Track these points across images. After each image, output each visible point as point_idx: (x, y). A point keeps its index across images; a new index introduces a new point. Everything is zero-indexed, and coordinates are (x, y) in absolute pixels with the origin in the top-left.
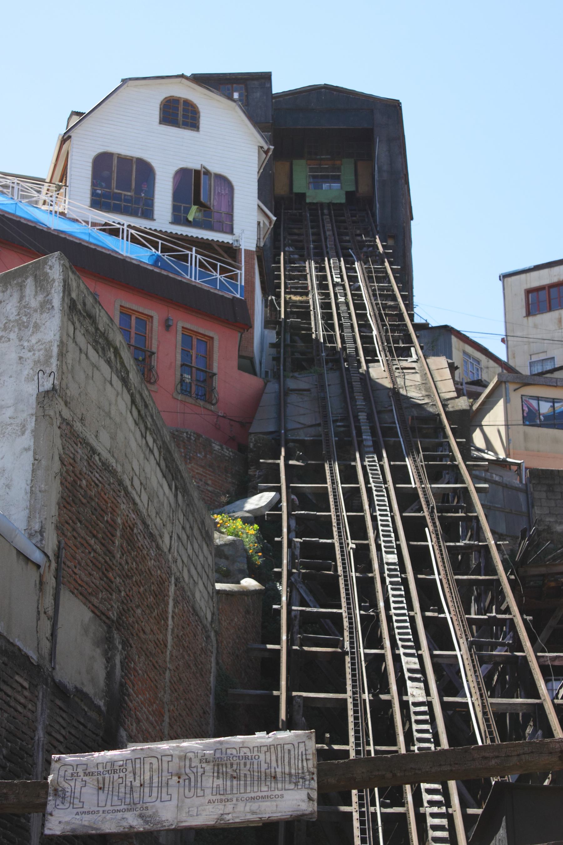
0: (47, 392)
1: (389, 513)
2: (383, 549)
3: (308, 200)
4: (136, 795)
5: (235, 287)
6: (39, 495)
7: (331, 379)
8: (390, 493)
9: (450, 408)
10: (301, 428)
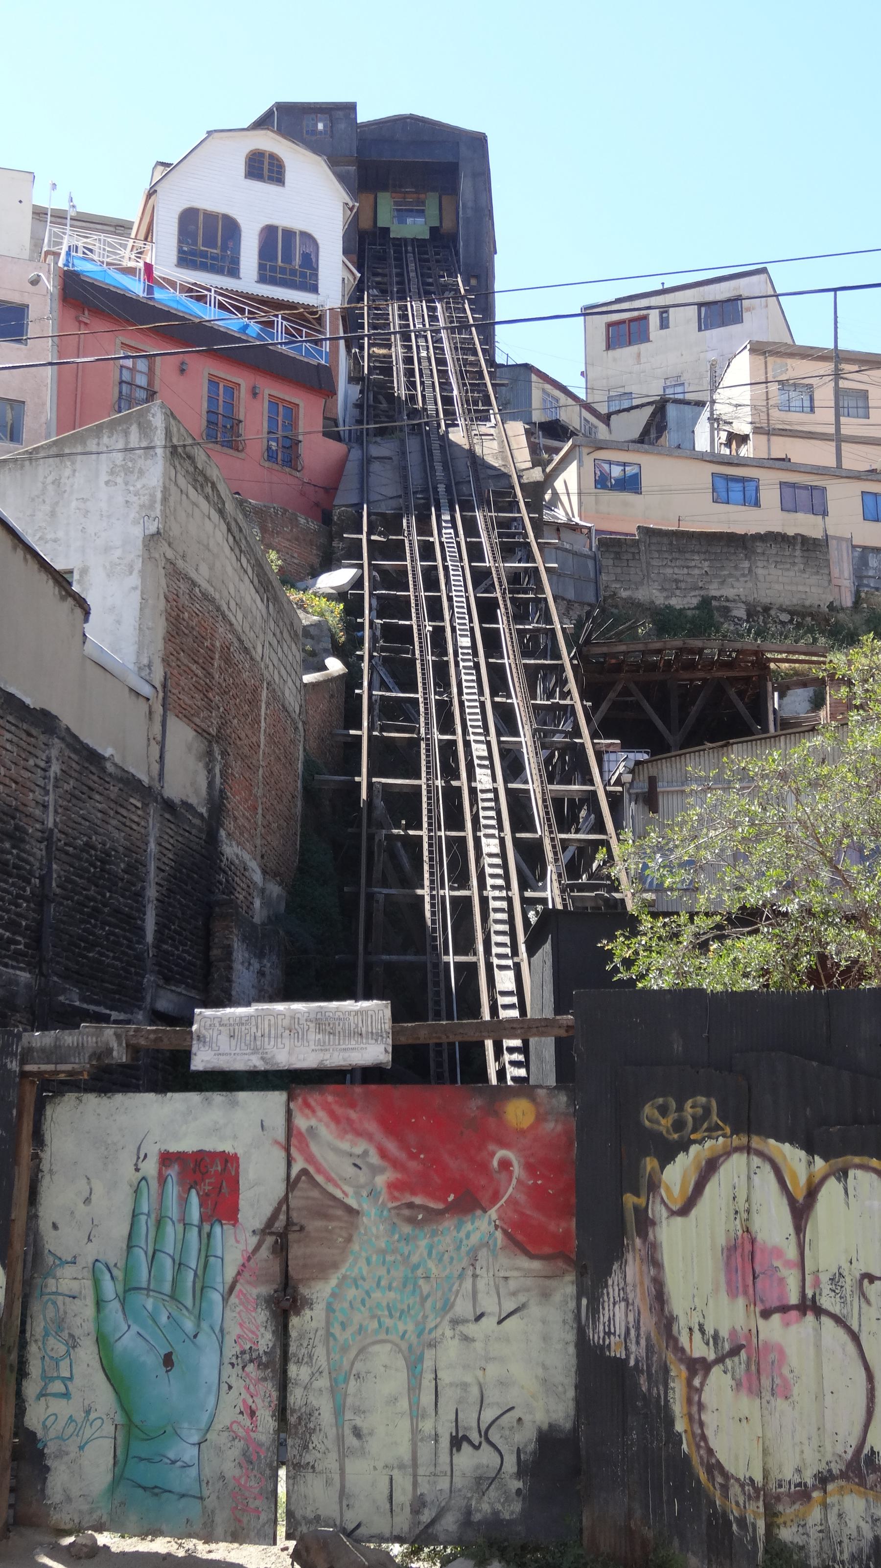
0: (153, 535)
4: (258, 1043)
5: (320, 353)
6: (147, 632)
9: (525, 480)
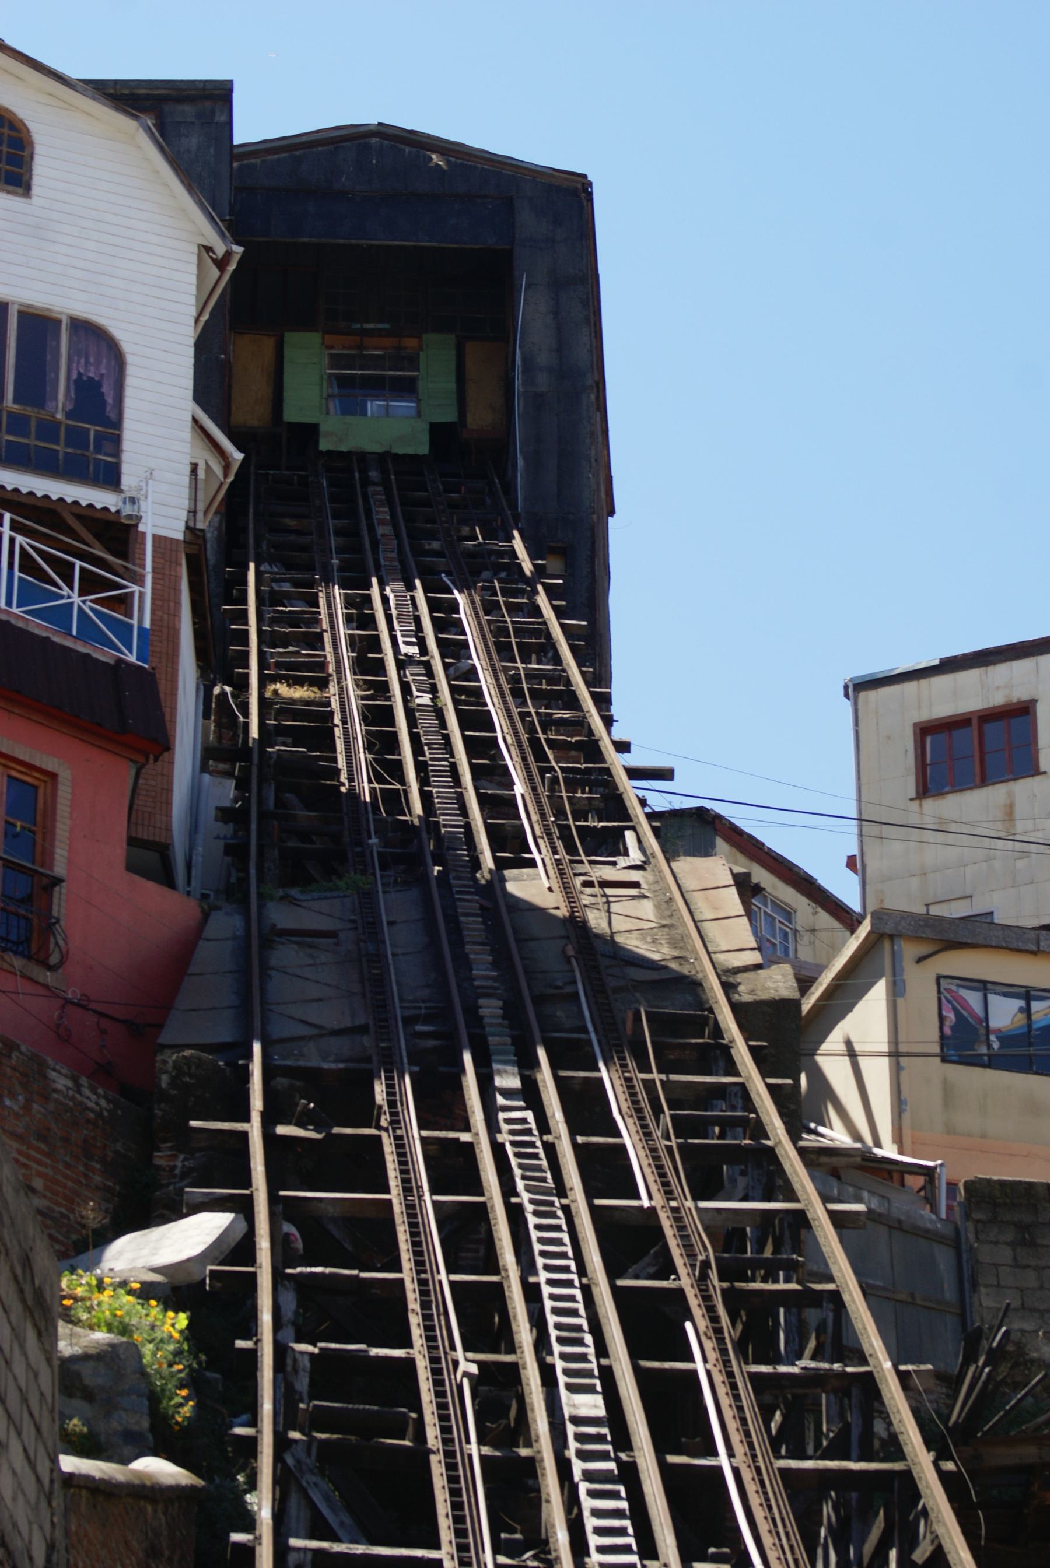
2: (562, 1380)
3: (324, 445)
5: (124, 631)
7: (396, 907)
8: (577, 1221)
9: (744, 995)
10: (311, 1038)
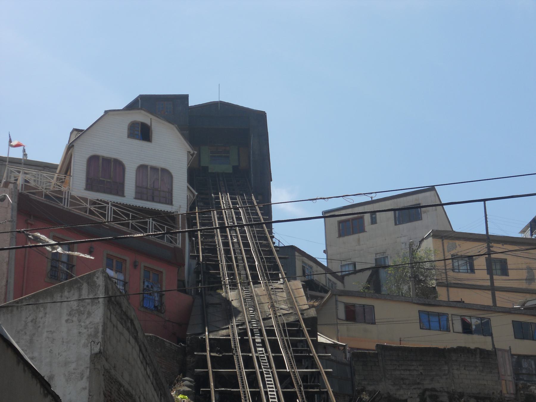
0: (96, 354)
1: (274, 389)
3: (210, 171)
9: (306, 316)
